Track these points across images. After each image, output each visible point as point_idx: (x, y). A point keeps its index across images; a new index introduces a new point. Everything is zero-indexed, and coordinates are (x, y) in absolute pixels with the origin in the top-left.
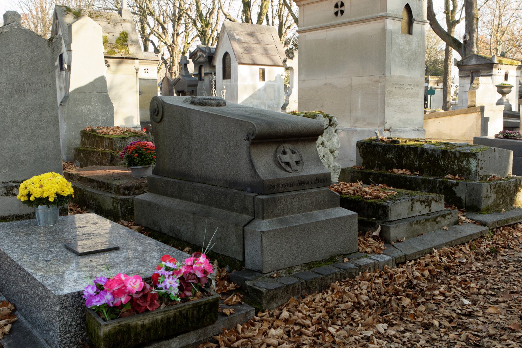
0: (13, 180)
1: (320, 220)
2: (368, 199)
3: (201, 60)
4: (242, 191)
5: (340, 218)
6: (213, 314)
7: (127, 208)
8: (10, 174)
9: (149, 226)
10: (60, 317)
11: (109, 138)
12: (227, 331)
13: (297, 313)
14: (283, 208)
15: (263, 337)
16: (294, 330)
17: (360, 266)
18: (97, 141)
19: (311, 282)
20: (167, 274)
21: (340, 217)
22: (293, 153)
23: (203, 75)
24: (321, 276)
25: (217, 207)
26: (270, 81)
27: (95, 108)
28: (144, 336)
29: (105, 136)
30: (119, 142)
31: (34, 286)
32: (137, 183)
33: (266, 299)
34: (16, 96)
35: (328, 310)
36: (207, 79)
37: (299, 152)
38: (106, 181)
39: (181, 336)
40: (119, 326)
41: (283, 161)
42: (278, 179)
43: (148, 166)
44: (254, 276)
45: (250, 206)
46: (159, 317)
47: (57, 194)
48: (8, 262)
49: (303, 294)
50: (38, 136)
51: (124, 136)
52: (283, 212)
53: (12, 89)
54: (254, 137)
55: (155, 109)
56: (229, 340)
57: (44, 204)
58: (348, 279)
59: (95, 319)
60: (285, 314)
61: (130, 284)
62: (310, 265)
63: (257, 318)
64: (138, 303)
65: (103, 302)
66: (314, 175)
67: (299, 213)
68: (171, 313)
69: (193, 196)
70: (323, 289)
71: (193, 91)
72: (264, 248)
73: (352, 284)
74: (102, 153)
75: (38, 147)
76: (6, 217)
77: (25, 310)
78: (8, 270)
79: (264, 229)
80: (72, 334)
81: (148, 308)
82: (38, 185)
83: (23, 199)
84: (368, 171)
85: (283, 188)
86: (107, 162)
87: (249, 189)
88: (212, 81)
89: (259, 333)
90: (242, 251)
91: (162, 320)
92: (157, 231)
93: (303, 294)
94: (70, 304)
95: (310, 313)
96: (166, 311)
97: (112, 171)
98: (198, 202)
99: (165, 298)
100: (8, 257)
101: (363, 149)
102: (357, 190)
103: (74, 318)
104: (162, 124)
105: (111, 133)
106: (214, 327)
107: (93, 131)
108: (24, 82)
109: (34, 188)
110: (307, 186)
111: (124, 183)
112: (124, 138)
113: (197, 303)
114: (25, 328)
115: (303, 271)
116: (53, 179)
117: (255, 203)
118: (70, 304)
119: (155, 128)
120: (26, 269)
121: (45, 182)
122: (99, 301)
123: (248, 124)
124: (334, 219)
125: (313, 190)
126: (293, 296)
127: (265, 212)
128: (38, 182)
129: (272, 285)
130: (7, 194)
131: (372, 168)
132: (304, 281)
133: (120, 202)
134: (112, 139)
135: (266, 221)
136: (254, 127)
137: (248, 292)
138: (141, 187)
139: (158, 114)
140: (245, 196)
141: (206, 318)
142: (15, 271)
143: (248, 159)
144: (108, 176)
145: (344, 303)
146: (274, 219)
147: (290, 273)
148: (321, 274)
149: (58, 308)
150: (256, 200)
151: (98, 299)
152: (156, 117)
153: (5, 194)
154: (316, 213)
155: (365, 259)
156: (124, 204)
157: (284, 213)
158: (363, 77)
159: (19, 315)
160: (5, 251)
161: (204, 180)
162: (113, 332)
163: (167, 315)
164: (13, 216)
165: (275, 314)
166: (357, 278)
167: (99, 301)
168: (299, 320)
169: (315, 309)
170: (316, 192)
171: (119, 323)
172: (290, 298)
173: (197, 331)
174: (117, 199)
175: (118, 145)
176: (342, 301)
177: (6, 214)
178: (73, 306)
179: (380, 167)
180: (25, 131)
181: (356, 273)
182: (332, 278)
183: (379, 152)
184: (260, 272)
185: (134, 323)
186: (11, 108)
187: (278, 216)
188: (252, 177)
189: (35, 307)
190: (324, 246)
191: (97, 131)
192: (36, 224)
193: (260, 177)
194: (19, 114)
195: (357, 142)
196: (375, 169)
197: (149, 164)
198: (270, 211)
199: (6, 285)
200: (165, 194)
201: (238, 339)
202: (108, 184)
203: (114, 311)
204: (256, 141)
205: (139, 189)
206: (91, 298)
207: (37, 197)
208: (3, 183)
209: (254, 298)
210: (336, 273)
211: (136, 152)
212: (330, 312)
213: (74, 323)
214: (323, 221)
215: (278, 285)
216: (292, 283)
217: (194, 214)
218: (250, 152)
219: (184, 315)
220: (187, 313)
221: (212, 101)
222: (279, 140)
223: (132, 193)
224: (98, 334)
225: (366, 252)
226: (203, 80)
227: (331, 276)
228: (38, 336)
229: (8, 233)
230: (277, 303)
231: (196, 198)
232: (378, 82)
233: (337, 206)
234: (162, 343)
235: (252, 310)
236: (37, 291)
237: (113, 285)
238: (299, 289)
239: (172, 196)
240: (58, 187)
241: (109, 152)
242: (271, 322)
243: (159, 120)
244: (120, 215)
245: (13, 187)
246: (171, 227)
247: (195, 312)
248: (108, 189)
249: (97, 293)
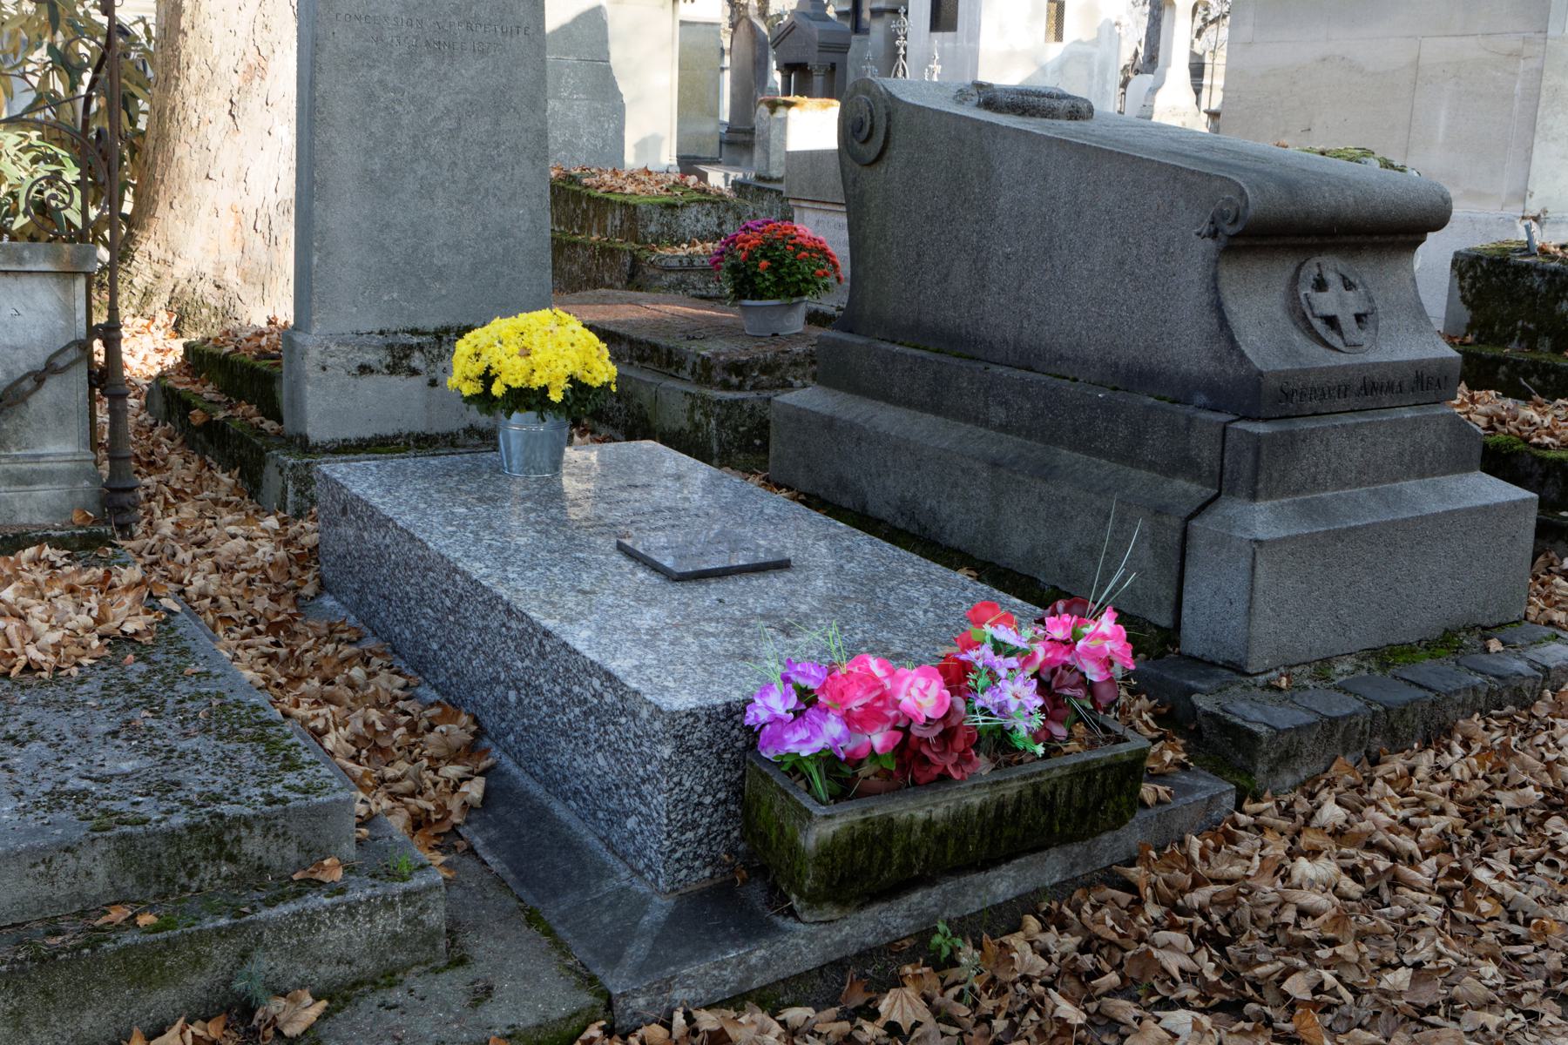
0: (410, 326)
1: (1427, 511)
2: (1547, 447)
4: (1173, 402)
5: (1486, 510)
6: (1124, 799)
7: (735, 430)
8: (402, 308)
9: (821, 492)
10: (671, 777)
11: (625, 205)
12: (1153, 854)
13: (1370, 812)
14: (1317, 466)
15: (1279, 883)
16: (1375, 869)
17: (1547, 669)
18: (585, 212)
19: (1403, 713)
20: (1002, 665)
21: (1487, 506)
22: (1349, 286)
23: (866, 15)
24: (1431, 695)
25: (1075, 450)
26: (1079, 42)
27: (570, 108)
28: (927, 857)
29: (612, 197)
30: (656, 216)
31: (567, 670)
32: (768, 353)
33: (1266, 759)
34: (429, 62)
35: (1464, 808)
36: (877, 28)
37: (1363, 284)
38: (663, 342)
39: (1023, 860)
40: (864, 821)
42: (1306, 372)
43: (795, 300)
44: (1215, 682)
45: (1207, 455)
46: (976, 801)
47: (572, 379)
48: (455, 584)
49: (1374, 749)
50: (487, 190)
51: (672, 201)
52: (1315, 479)
53: (417, 38)
54: (1239, 228)
55: (862, 123)
56: (1168, 884)
57: (529, 408)
58: (1509, 709)
59: (787, 795)
60: (1332, 813)
61: (908, 694)
62: (1384, 656)
63: (1243, 819)
64: (916, 757)
65: (819, 744)
66: (1412, 364)
67: (1360, 485)
68: (1011, 791)
69: (987, 406)
70: (1437, 736)
71: (833, 66)
72: (1258, 595)
73: (1525, 728)
74: (603, 250)
75: (485, 227)
76: (387, 438)
77: (520, 739)
78: (452, 611)
79: (1261, 533)
80: (701, 831)
81: (952, 771)
82: (517, 350)
83: (468, 389)
84: (1488, 351)
85: (1315, 402)
86: (618, 279)
87: (1201, 399)
88: (897, 37)
89: (1262, 869)
90: (1172, 598)
91: (982, 811)
92: (849, 510)
93: (1374, 749)
94: (700, 739)
95: (1407, 812)
96: (997, 783)
97: (669, 309)
98: (1004, 428)
99: (1000, 742)
100: (456, 570)
101: (1475, 278)
102: (1498, 416)
103: (709, 783)
104: (881, 169)
105: (629, 190)
106: (1116, 839)
107: (572, 179)
108: (454, 19)
109: (504, 358)
110: (1386, 399)
111: (724, 349)
112: (671, 206)
113: (1087, 763)
114: (526, 795)
115: (1364, 673)
116: (557, 330)
117: (1229, 445)
118: (700, 739)
119: (855, 182)
120: (532, 614)
121: (536, 340)
122: (807, 741)
123: (1218, 183)
124: (1469, 511)
125: (1408, 414)
126: (1344, 754)
127: (1263, 476)
128: (514, 338)
129: (1286, 717)
130: (393, 369)
131: (1503, 342)
132: (1381, 709)
133: (717, 410)
134: (635, 207)
135: (1261, 505)
136: (1242, 193)
137: (1199, 730)
138: (779, 366)
139: (870, 136)
140: (1190, 420)
141: (1104, 812)
142: (483, 618)
143: (1205, 298)
144: (659, 325)
145: (1514, 787)
146: (1285, 501)
147: (1327, 679)
148: (1430, 690)
149: (667, 751)
150: (1231, 435)
151: (803, 733)
152: (862, 148)
153: (388, 367)
154: (1410, 486)
155: (1555, 646)
156: (728, 417)
157: (1316, 484)
158: (1464, 40)
159: (496, 753)
160: (444, 551)
161: (1027, 359)
162: (843, 839)
163: (998, 795)
164: (408, 435)
165: (1298, 808)
166: (1541, 709)
167: (807, 741)
168: (1380, 837)
169: (1422, 801)
170: (1415, 420)
171: (864, 813)
172: (1335, 758)
173: (1068, 848)
174: (705, 400)
175: (653, 228)
176: (1506, 781)
177: (389, 430)
178: (710, 747)
179: (1530, 340)
180: (449, 174)
181: (1533, 693)
182: (1462, 705)
183: (1532, 293)
184: (1238, 669)
185: (905, 815)
186: (412, 100)
187: (1297, 492)
188: (1220, 360)
189: (563, 733)
190: (1429, 597)
191: (585, 181)
192: (497, 470)
193: (1250, 362)
194: (436, 120)
195: (1457, 254)
196: (1515, 344)
197: (800, 294)
198: (1275, 475)
199: (443, 653)
200: (882, 394)
201: (1198, 882)
202: (670, 351)
203: (840, 775)
204: (1242, 242)
205: (775, 373)
206: (778, 727)
207: (514, 385)
208: (381, 333)
209: (1226, 749)
210: (1475, 689)
211: (764, 256)
212: (1472, 811)
213: (708, 800)
214: (1436, 516)
215: (1304, 718)
216: (1347, 711)
217: (995, 464)
218: (1215, 278)
219: (1044, 798)
220: (1053, 793)
221: (1056, 103)
222: (1309, 241)
223: (749, 383)
224: (793, 840)
225: (1550, 623)
226: (867, 32)
227: (1459, 698)
228: (574, 825)
229: (425, 492)
230: (1295, 772)
231: (998, 414)
232: (1516, 55)
233: (1473, 470)
234: (968, 878)
235: (1226, 791)
236: (576, 689)
237: (848, 694)
238: (1363, 733)
239: (907, 403)
240: (577, 358)
241: (626, 246)
242: (1290, 833)
243: (872, 156)
244: (716, 449)
245: (411, 347)
246: (903, 499)
247: (1077, 790)
248: (669, 364)
249: (798, 714)
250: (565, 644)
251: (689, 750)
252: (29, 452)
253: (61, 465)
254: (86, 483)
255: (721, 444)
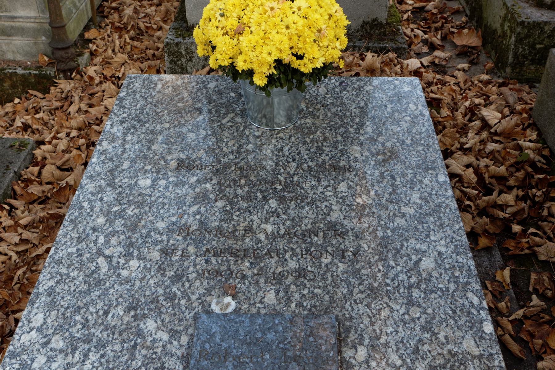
7: (533, 46)
133: (519, 30)
156: (527, 36)
250: (439, 127)
252: (8, 14)
253: (29, 25)
254: (44, 38)
255: (516, 56)
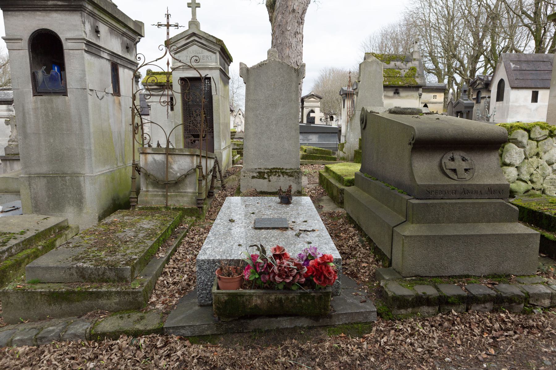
3: (480, 87)
14: (438, 215)
34: (270, 109)
41: (447, 168)
97: (343, 167)
251: (203, 270)
